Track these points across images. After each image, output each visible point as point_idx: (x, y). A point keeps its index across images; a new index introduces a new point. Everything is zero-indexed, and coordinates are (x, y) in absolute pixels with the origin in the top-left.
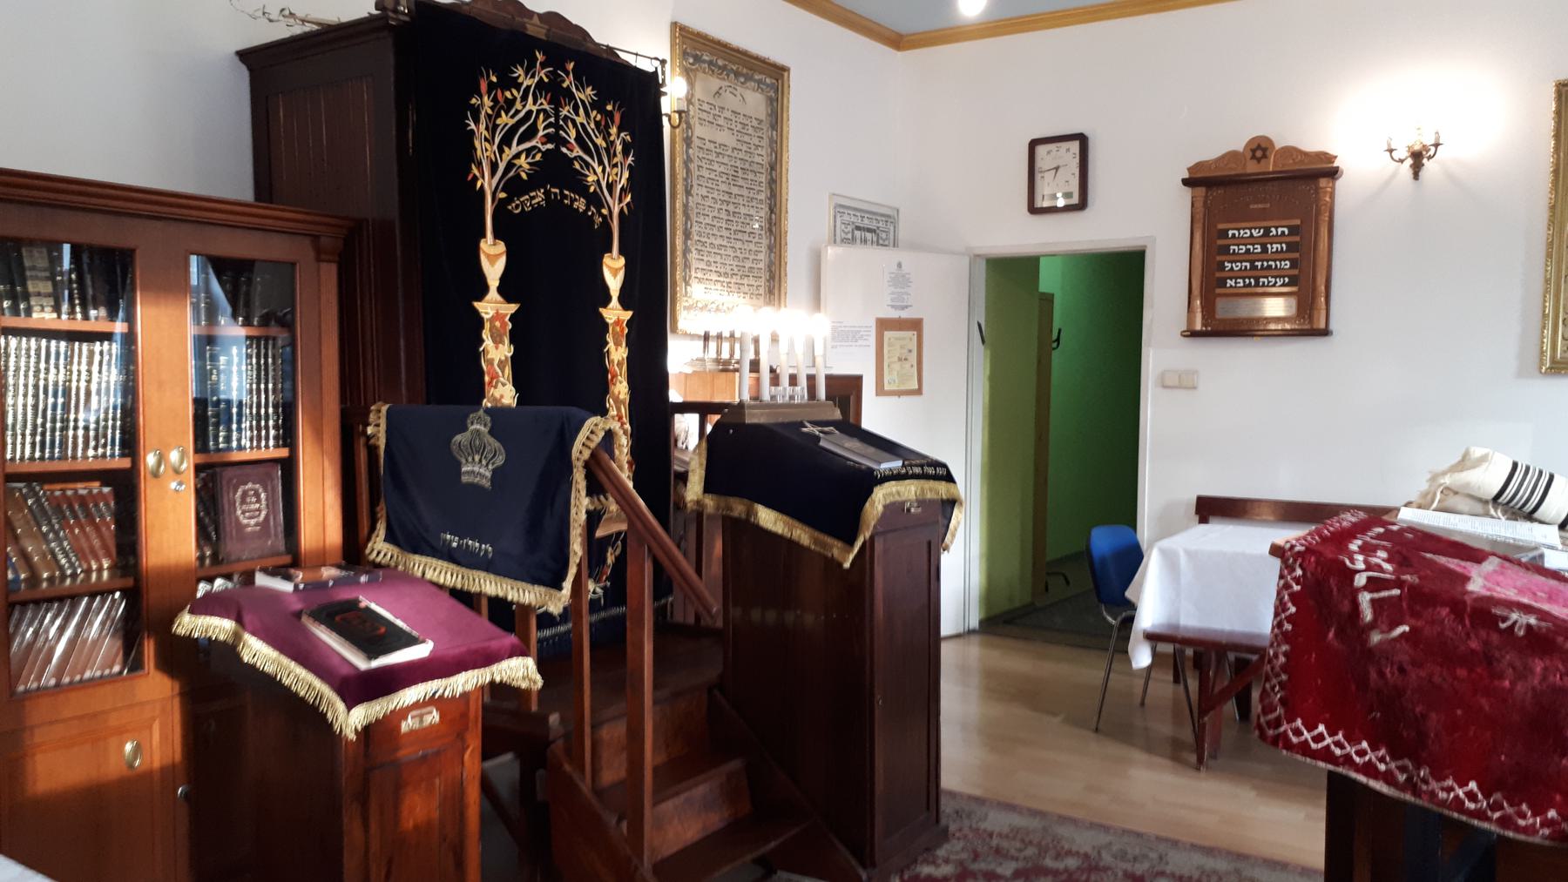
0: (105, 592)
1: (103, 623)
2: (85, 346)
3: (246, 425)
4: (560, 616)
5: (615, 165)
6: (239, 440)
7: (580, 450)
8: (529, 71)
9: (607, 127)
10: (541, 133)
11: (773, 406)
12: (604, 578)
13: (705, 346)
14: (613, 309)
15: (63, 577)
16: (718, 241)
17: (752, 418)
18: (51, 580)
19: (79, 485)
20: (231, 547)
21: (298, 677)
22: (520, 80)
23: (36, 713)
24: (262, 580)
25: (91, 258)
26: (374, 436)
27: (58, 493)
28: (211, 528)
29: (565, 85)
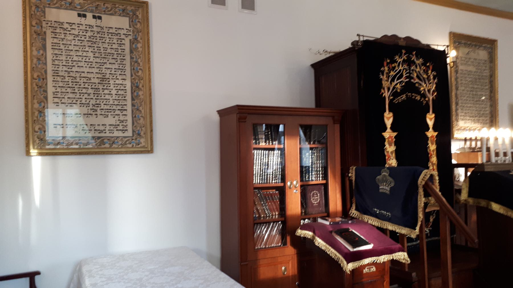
0: (275, 222)
1: (276, 230)
2: (272, 152)
3: (313, 173)
4: (416, 238)
5: (430, 83)
6: (312, 178)
7: (421, 181)
8: (400, 57)
9: (427, 71)
10: (404, 76)
11: (496, 164)
12: (429, 226)
13: (465, 143)
14: (388, 132)
15: (267, 217)
16: (469, 105)
17: (487, 169)
18: (264, 217)
19: (270, 191)
20: (310, 210)
21: (332, 252)
22: (397, 60)
23: (261, 255)
24: (320, 220)
25: (274, 128)
26: (351, 177)
27: (268, 193)
28: (304, 204)
29: (412, 59)
